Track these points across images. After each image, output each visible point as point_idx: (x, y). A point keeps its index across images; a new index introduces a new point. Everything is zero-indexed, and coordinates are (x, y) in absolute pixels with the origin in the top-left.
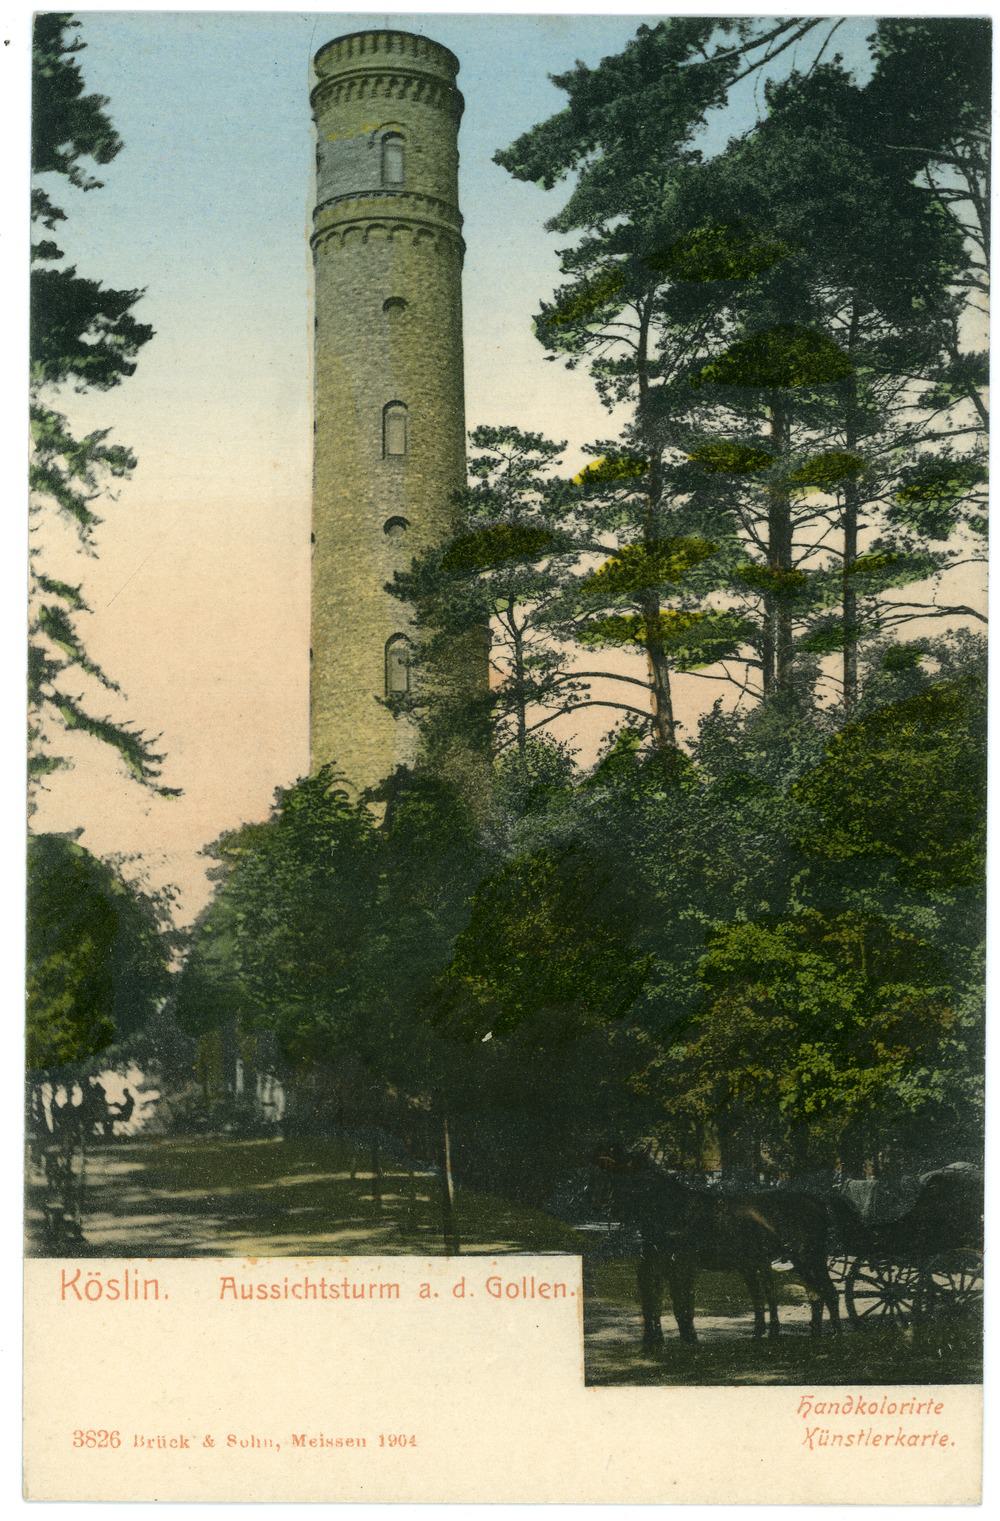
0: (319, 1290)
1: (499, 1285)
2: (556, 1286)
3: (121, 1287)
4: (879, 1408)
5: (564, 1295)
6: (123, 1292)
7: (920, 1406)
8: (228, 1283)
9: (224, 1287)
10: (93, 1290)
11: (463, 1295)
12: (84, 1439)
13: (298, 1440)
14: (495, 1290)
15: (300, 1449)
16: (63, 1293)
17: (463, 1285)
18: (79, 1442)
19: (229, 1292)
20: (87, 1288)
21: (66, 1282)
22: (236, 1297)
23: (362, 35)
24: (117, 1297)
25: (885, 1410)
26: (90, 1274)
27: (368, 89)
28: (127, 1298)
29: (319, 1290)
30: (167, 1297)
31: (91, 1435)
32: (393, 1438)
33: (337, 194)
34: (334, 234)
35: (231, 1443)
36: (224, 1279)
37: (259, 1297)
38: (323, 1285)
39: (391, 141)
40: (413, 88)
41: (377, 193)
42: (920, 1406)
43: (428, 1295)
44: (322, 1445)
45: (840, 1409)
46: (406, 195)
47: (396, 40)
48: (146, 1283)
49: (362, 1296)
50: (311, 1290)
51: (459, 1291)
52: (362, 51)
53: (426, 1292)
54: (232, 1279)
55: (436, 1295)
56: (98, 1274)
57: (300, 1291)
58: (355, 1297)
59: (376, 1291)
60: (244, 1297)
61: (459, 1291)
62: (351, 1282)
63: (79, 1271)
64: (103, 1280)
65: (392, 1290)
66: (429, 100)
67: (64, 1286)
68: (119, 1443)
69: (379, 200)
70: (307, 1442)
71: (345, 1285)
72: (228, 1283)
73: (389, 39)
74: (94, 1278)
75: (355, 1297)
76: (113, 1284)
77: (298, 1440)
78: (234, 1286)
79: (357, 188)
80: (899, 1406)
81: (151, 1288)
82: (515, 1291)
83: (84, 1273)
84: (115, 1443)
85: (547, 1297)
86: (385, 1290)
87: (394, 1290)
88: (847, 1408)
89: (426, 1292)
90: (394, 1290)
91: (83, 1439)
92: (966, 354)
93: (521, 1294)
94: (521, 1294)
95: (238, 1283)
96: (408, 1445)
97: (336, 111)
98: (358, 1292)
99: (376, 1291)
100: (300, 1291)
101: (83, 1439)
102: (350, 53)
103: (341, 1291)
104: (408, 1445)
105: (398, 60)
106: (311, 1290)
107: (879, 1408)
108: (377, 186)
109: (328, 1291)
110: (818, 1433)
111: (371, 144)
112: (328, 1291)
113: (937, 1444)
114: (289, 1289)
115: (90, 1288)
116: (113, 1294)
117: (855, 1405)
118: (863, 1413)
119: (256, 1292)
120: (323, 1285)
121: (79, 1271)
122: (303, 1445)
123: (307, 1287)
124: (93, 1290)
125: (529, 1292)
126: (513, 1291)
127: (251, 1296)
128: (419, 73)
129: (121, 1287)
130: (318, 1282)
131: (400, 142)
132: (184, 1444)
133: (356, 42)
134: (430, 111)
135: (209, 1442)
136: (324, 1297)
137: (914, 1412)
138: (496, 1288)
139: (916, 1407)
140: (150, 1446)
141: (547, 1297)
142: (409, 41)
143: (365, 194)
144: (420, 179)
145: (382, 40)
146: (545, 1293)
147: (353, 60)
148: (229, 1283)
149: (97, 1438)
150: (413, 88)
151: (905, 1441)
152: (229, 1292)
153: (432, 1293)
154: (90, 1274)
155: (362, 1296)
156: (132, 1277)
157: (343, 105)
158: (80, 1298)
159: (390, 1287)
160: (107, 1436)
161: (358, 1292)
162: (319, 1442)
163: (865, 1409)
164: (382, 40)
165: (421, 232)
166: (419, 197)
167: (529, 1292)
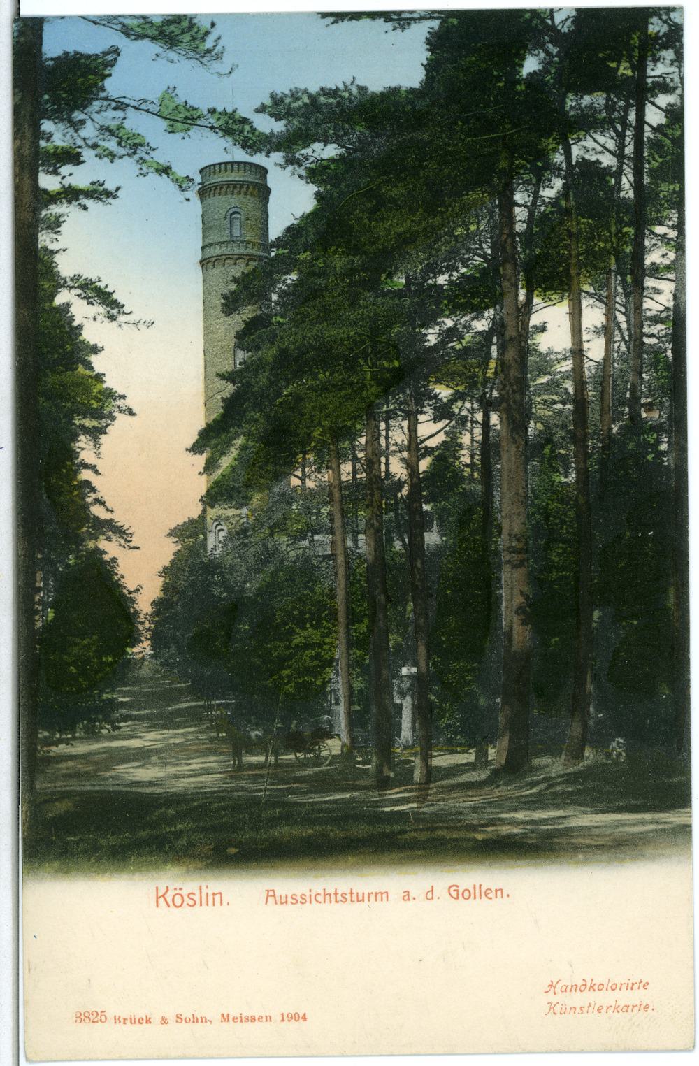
0: (333, 896)
1: (457, 891)
2: (496, 891)
3: (197, 898)
4: (605, 986)
5: (221, 904)
6: (198, 902)
7: (633, 984)
8: (270, 894)
9: (268, 896)
10: (178, 901)
11: (432, 898)
12: (83, 1017)
13: (225, 1018)
14: (454, 894)
15: (225, 1024)
16: (157, 901)
17: (432, 890)
18: (79, 1020)
19: (271, 900)
20: (173, 898)
21: (159, 895)
22: (276, 903)
23: (220, 164)
24: (193, 906)
25: (609, 988)
26: (175, 889)
27: (223, 191)
28: (201, 905)
29: (333, 896)
30: (508, 896)
31: (87, 1015)
32: (290, 1016)
33: (211, 242)
34: (209, 262)
35: (179, 1020)
36: (268, 891)
37: (292, 903)
38: (336, 894)
39: (234, 216)
40: (244, 189)
41: (229, 242)
42: (633, 984)
43: (409, 899)
44: (241, 1021)
45: (578, 989)
46: (242, 242)
47: (236, 166)
48: (214, 894)
49: (363, 900)
50: (327, 897)
51: (430, 895)
52: (220, 171)
53: (407, 896)
54: (274, 891)
55: (414, 899)
56: (181, 889)
57: (320, 898)
58: (358, 901)
59: (372, 897)
60: (281, 903)
61: (430, 895)
62: (340, 892)
63: (167, 888)
64: (184, 892)
65: (382, 895)
66: (252, 195)
67: (158, 898)
68: (106, 1019)
69: (229, 245)
70: (231, 1019)
71: (351, 893)
72: (270, 894)
73: (239, 166)
74: (178, 891)
75: (358, 901)
76: (192, 896)
77: (225, 1018)
78: (274, 896)
79: (219, 240)
80: (619, 986)
81: (218, 898)
82: (467, 895)
83: (171, 888)
84: (103, 1018)
85: (491, 898)
86: (379, 896)
87: (384, 896)
88: (583, 988)
89: (407, 896)
90: (384, 896)
91: (83, 1017)
92: (313, 188)
93: (472, 896)
94: (472, 896)
95: (277, 894)
96: (301, 1020)
97: (210, 201)
98: (360, 898)
99: (372, 897)
100: (320, 898)
101: (83, 1017)
102: (215, 173)
103: (348, 897)
104: (301, 1020)
105: (235, 176)
106: (327, 897)
107: (605, 986)
108: (226, 239)
109: (339, 897)
110: (560, 1005)
111: (225, 218)
112: (339, 897)
113: (642, 1011)
114: (313, 897)
115: (176, 899)
116: (191, 903)
117: (588, 986)
118: (594, 990)
119: (290, 900)
120: (336, 894)
121: (167, 888)
122: (228, 1021)
123: (325, 895)
124: (178, 901)
125: (478, 895)
126: (466, 894)
127: (286, 902)
128: (247, 182)
129: (197, 898)
130: (332, 892)
131: (239, 216)
132: (148, 1021)
133: (217, 168)
134: (252, 199)
135: (164, 1021)
136: (337, 902)
137: (629, 988)
138: (456, 893)
139: (630, 985)
140: (124, 1023)
141: (491, 898)
142: (242, 165)
143: (223, 243)
144: (249, 234)
145: (229, 166)
146: (489, 896)
147: (215, 176)
148: (271, 893)
149: (91, 1016)
150: (244, 189)
151: (619, 1009)
152: (271, 900)
153: (411, 898)
154: (175, 889)
155: (363, 900)
156: (204, 891)
157: (212, 198)
158: (169, 906)
159: (382, 894)
160: (98, 1014)
161: (360, 898)
162: (239, 1020)
163: (596, 987)
164: (229, 166)
165: (249, 260)
166: (248, 243)
167: (478, 895)
